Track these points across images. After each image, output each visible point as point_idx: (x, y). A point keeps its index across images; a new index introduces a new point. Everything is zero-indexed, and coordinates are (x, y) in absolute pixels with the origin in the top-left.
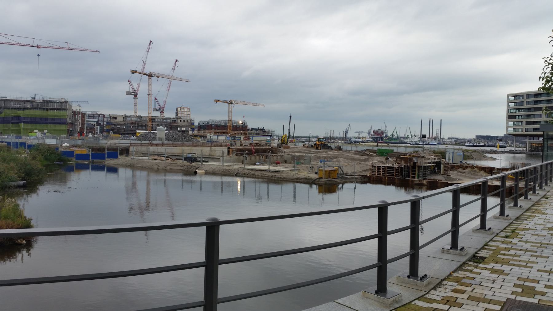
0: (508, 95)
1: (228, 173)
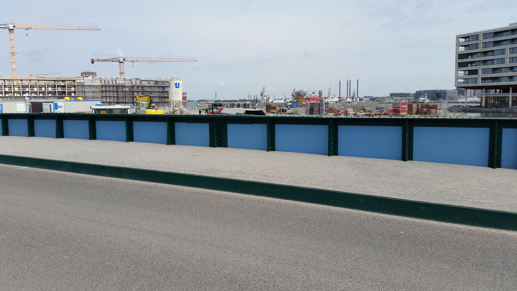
0: (457, 36)
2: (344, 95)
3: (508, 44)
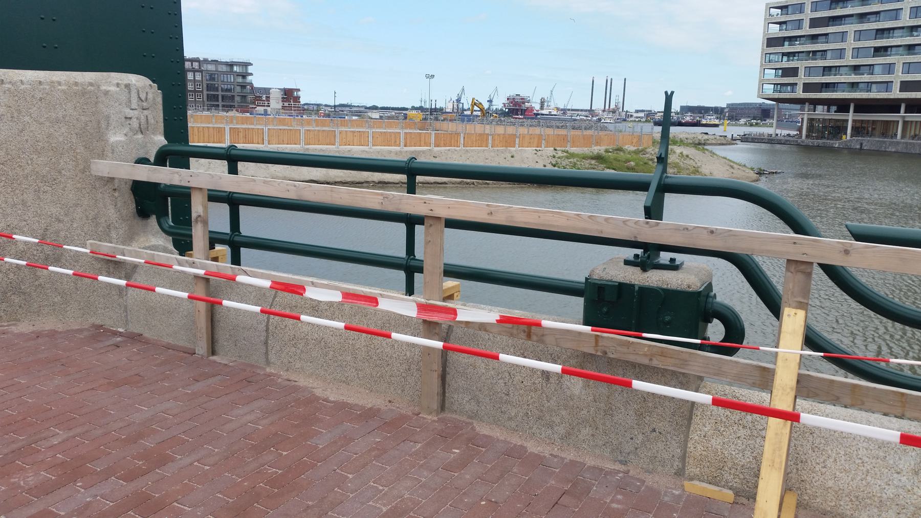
0: (767, 4)
1: (635, 115)
2: (598, 105)
3: (852, 24)
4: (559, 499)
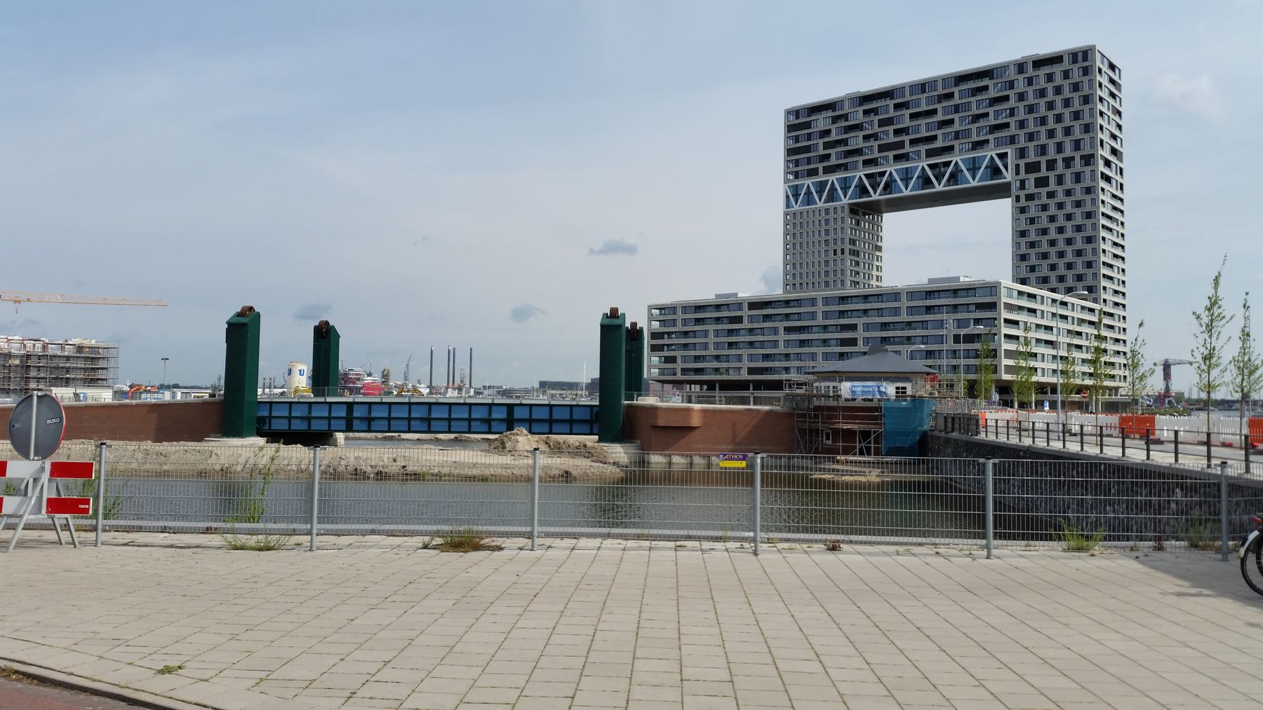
0: (649, 306)
4: (379, 670)
